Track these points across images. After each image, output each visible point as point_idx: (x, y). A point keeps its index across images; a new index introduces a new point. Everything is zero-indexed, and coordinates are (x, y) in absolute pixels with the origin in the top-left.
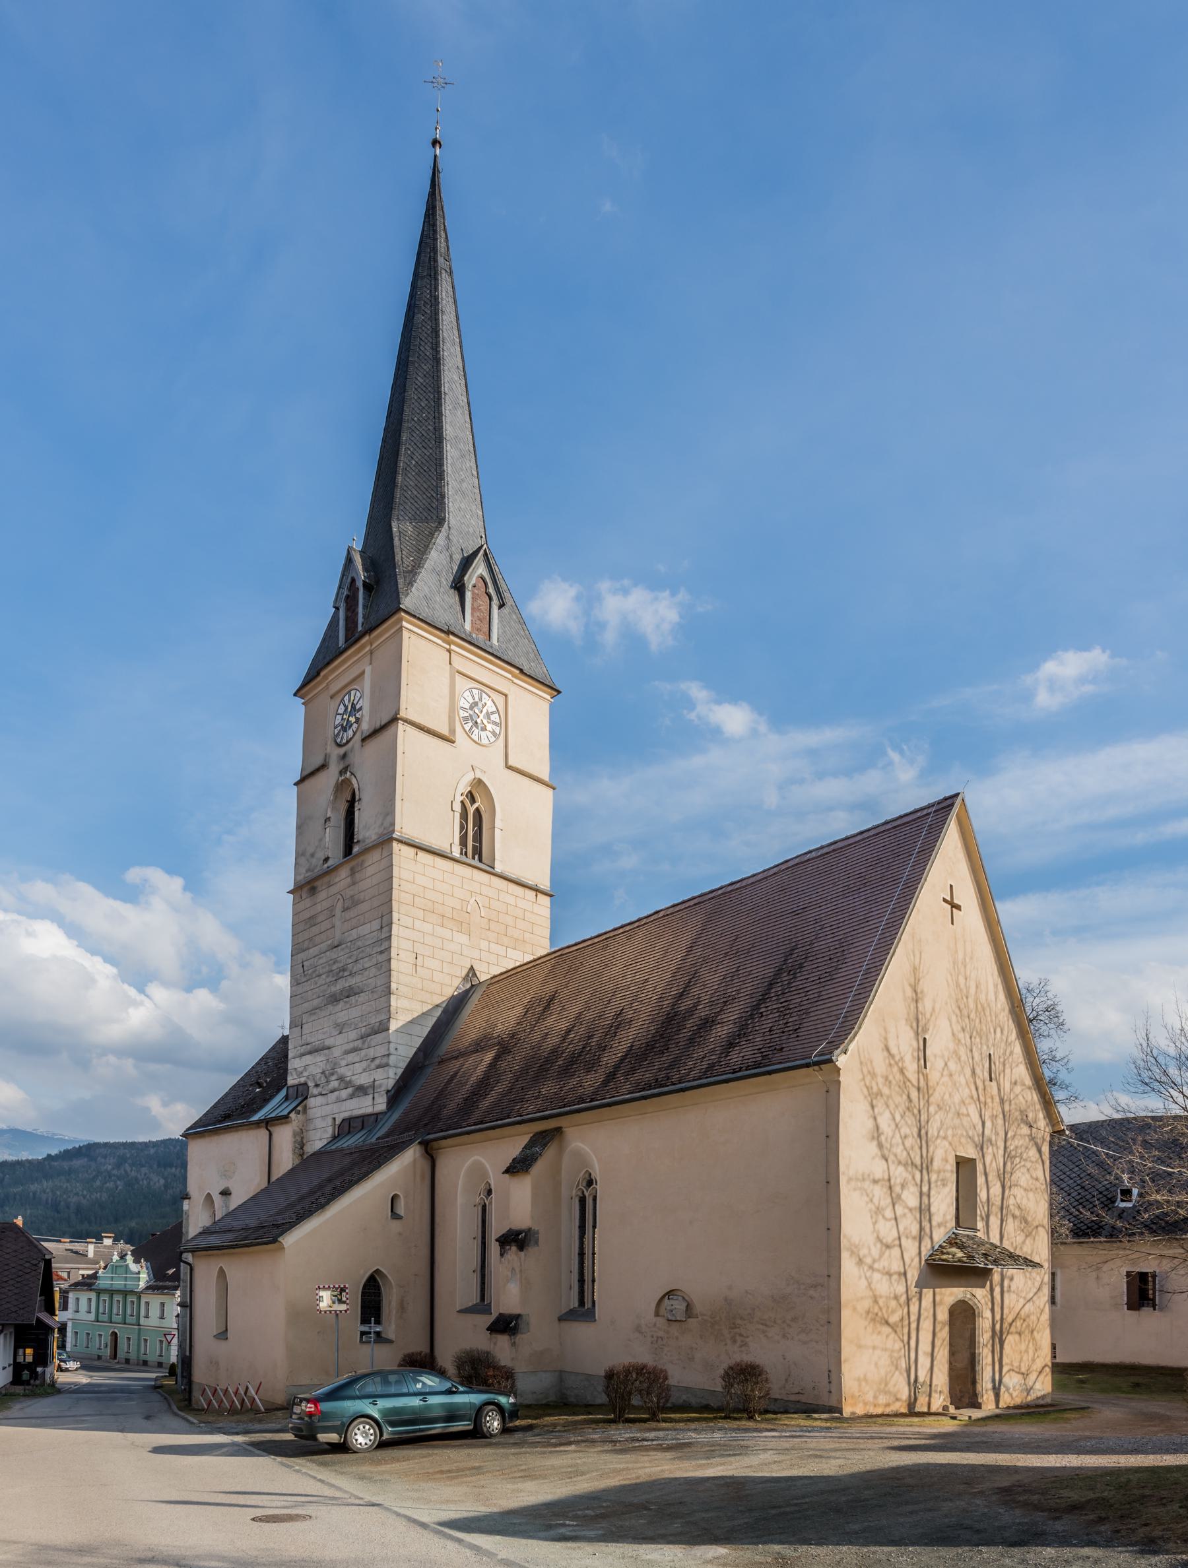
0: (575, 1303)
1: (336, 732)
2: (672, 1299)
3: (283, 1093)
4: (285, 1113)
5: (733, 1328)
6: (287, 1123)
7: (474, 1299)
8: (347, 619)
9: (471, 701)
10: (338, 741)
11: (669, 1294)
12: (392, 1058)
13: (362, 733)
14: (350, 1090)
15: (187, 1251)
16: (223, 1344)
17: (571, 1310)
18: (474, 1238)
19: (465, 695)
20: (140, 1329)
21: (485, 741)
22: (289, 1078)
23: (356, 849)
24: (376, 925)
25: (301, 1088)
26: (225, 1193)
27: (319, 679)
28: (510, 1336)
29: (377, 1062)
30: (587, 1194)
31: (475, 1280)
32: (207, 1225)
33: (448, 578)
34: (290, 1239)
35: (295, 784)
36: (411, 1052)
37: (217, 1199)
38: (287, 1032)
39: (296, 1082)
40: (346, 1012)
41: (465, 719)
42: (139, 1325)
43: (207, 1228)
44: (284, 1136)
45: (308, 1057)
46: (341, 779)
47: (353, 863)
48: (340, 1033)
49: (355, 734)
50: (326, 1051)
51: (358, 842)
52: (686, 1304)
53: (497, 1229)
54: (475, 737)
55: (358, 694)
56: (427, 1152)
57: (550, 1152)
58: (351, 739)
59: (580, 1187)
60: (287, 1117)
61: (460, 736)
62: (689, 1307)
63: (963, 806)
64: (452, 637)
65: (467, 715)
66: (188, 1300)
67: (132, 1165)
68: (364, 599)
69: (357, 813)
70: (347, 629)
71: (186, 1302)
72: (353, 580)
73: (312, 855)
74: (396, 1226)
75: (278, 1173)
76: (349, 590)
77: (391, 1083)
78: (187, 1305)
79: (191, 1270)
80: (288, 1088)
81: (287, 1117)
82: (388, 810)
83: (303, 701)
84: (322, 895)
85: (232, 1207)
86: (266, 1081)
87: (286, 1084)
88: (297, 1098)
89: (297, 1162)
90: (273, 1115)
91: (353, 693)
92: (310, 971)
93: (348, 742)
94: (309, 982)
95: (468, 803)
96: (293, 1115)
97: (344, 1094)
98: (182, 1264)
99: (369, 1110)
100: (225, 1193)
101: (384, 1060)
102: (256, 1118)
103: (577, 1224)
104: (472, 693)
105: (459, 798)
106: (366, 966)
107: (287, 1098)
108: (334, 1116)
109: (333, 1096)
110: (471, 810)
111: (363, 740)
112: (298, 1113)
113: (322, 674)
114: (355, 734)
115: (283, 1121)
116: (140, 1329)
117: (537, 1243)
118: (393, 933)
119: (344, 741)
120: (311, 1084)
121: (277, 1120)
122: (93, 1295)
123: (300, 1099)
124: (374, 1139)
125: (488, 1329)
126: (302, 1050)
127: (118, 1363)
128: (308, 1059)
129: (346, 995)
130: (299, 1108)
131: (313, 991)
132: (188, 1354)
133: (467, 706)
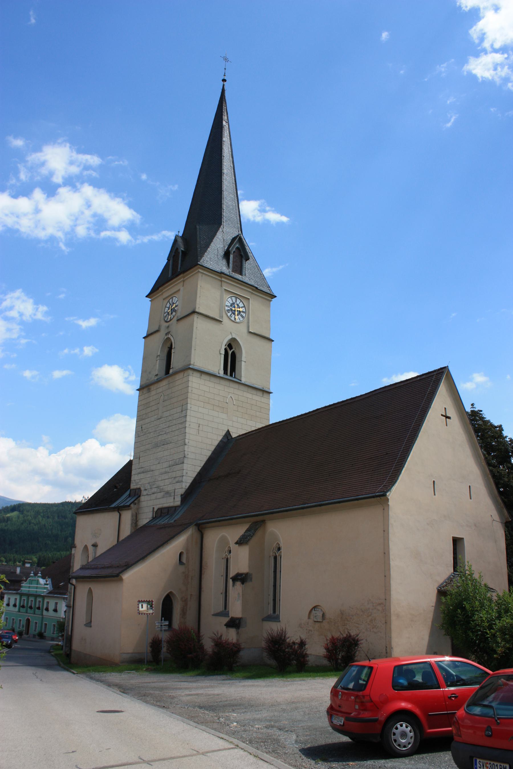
0: (271, 612)
1: (165, 315)
2: (316, 610)
3: (128, 493)
4: (128, 504)
5: (344, 626)
6: (128, 509)
7: (221, 608)
8: (173, 265)
9: (231, 302)
10: (166, 319)
11: (315, 607)
12: (184, 477)
13: (177, 317)
14: (162, 494)
15: (73, 578)
16: (88, 628)
17: (269, 615)
18: (222, 576)
19: (228, 300)
20: (43, 618)
21: (238, 320)
22: (132, 485)
23: (171, 371)
24: (179, 409)
25: (137, 490)
26: (95, 546)
27: (158, 291)
28: (236, 629)
29: (177, 479)
30: (277, 555)
31: (222, 598)
32: (84, 564)
33: (222, 253)
34: (128, 576)
35: (143, 338)
36: (194, 475)
37: (91, 549)
38: (132, 459)
39: (135, 487)
40: (162, 452)
41: (228, 310)
42: (42, 615)
43: (84, 566)
44: (127, 516)
45: (142, 474)
46: (166, 337)
47: (170, 379)
48: (159, 463)
49: (174, 317)
50: (151, 472)
51: (173, 368)
52: (322, 613)
53: (232, 574)
54: (233, 319)
55: (176, 299)
56: (199, 529)
57: (259, 533)
58: (172, 319)
59: (274, 551)
60: (129, 506)
61: (225, 320)
62: (323, 615)
63: (443, 662)
64: (222, 275)
65: (229, 309)
66: (72, 603)
67: (43, 517)
68: (182, 257)
69: (172, 354)
70: (173, 269)
71: (71, 604)
72: (177, 249)
73: (150, 373)
74: (182, 568)
75: (123, 537)
76: (175, 253)
77: (182, 491)
78: (71, 607)
79: (75, 588)
80: (131, 490)
81: (129, 506)
82: (188, 355)
83: (150, 299)
84: (153, 393)
85: (98, 555)
86: (120, 485)
87: (130, 488)
88: (135, 496)
89: (133, 531)
90: (122, 505)
91: (174, 298)
92: (145, 431)
93: (170, 320)
94: (144, 436)
95: (228, 349)
96: (132, 505)
97: (160, 495)
98: (69, 585)
99: (172, 504)
100: (95, 546)
101: (180, 479)
102: (113, 506)
103: (273, 570)
104: (232, 299)
105: (224, 347)
106: (173, 430)
107: (130, 495)
108: (153, 507)
109: (153, 496)
110: (230, 352)
111: (178, 320)
112: (135, 504)
113: (160, 289)
114: (174, 317)
115: (127, 508)
116: (43, 618)
117: (251, 580)
118: (187, 414)
119: (169, 320)
120: (142, 489)
121: (124, 507)
122: (18, 597)
123: (137, 496)
124: (173, 521)
125: (225, 625)
126: (139, 471)
127: (29, 637)
128: (142, 476)
129: (163, 444)
130: (136, 502)
131: (146, 440)
132: (70, 633)
133: (229, 305)
